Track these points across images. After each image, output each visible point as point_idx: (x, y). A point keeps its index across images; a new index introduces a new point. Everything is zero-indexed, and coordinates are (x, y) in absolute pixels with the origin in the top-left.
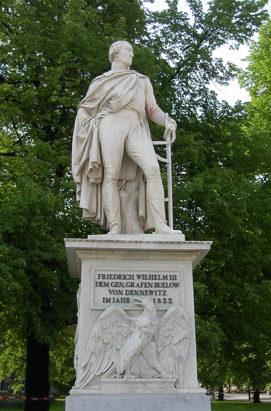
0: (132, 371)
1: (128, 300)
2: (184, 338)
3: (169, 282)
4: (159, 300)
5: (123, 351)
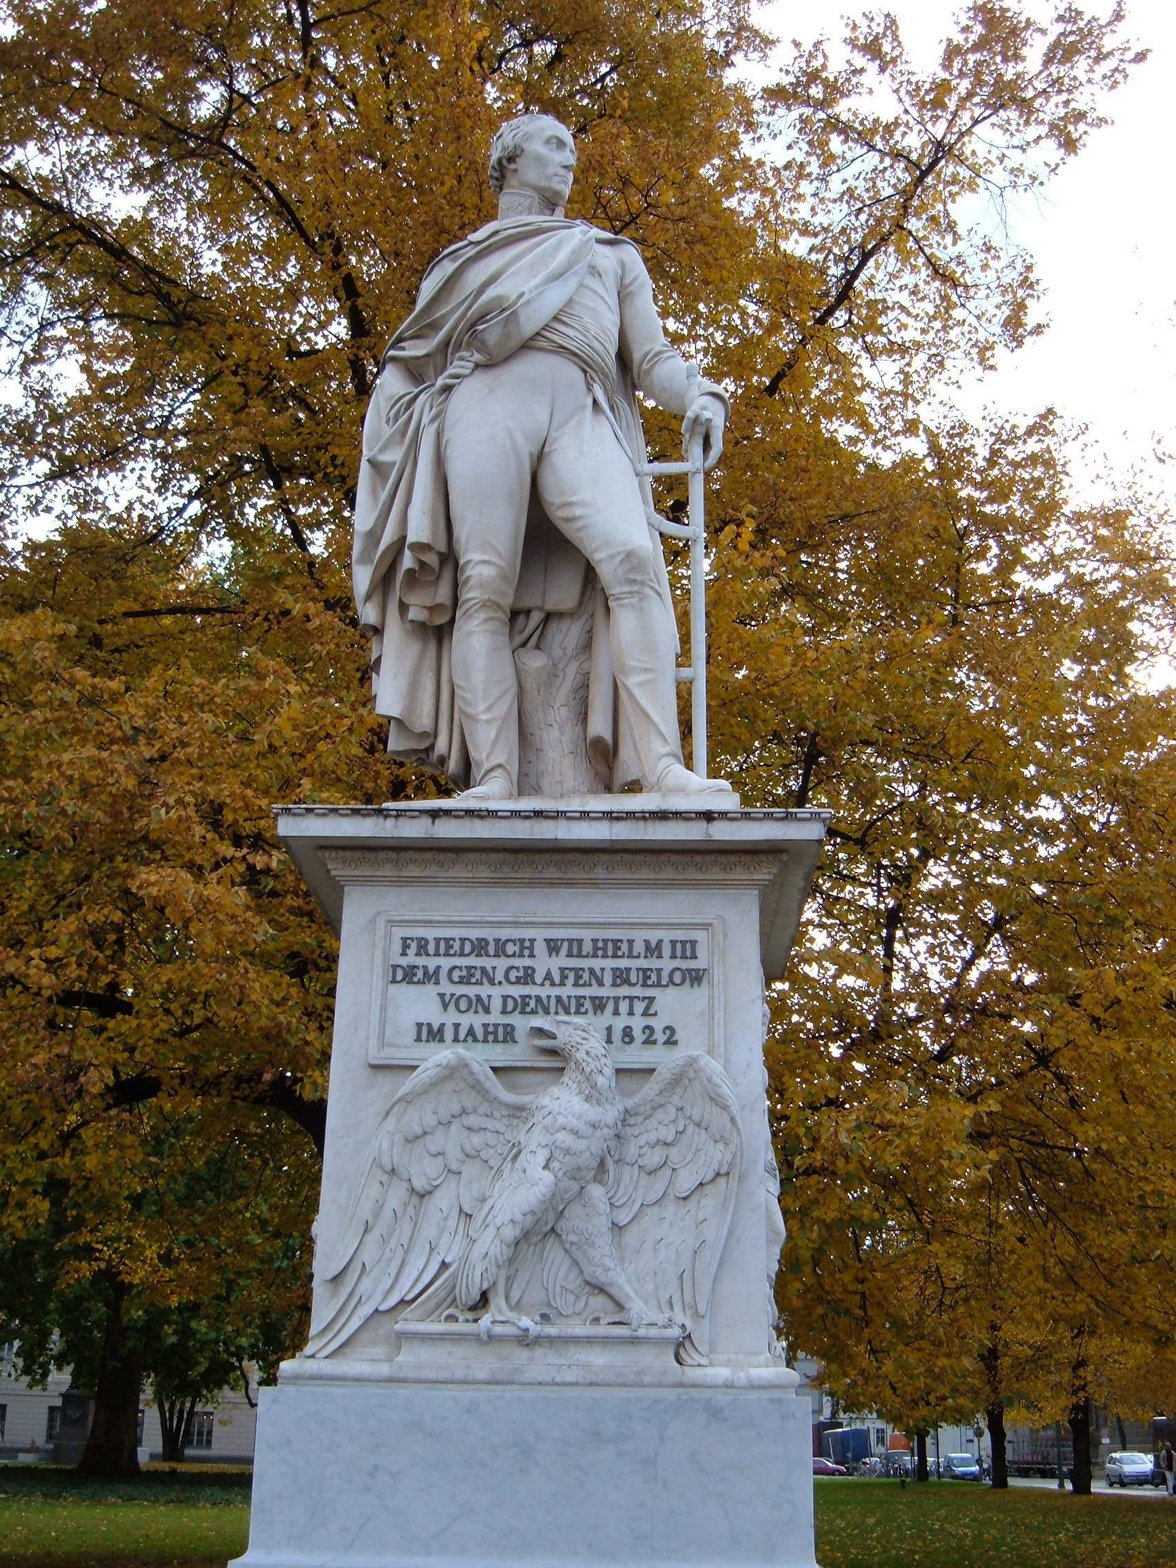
0: (515, 1295)
1: (509, 1035)
2: (718, 1174)
3: (667, 964)
4: (628, 1033)
5: (480, 1221)
